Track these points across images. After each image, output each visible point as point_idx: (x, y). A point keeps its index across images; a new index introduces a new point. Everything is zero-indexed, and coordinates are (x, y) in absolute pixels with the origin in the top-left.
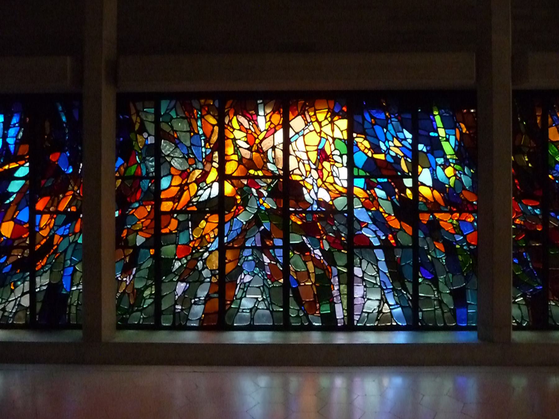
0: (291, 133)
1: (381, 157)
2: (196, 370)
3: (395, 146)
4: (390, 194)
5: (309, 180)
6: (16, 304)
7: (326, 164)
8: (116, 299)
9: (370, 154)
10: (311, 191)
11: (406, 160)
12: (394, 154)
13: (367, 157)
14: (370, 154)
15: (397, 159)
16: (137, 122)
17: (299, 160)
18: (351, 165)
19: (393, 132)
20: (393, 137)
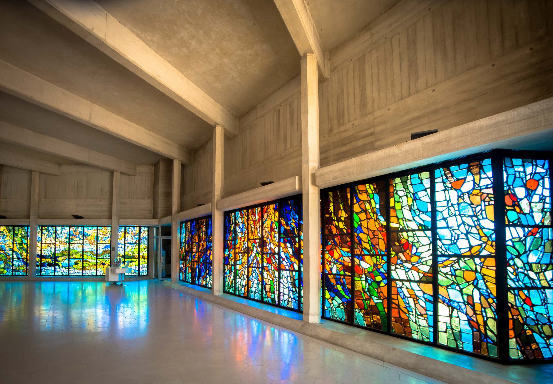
0: (264, 220)
1: (288, 228)
2: (336, 349)
3: (293, 222)
4: (292, 245)
5: (268, 240)
6: (534, 334)
7: (273, 232)
8: (302, 303)
9: (285, 227)
10: (477, 231)
11: (296, 229)
12: (292, 226)
13: (493, 206)
14: (285, 227)
15: (293, 228)
16: (516, 177)
17: (266, 231)
18: (279, 233)
19: (292, 216)
20: (292, 218)
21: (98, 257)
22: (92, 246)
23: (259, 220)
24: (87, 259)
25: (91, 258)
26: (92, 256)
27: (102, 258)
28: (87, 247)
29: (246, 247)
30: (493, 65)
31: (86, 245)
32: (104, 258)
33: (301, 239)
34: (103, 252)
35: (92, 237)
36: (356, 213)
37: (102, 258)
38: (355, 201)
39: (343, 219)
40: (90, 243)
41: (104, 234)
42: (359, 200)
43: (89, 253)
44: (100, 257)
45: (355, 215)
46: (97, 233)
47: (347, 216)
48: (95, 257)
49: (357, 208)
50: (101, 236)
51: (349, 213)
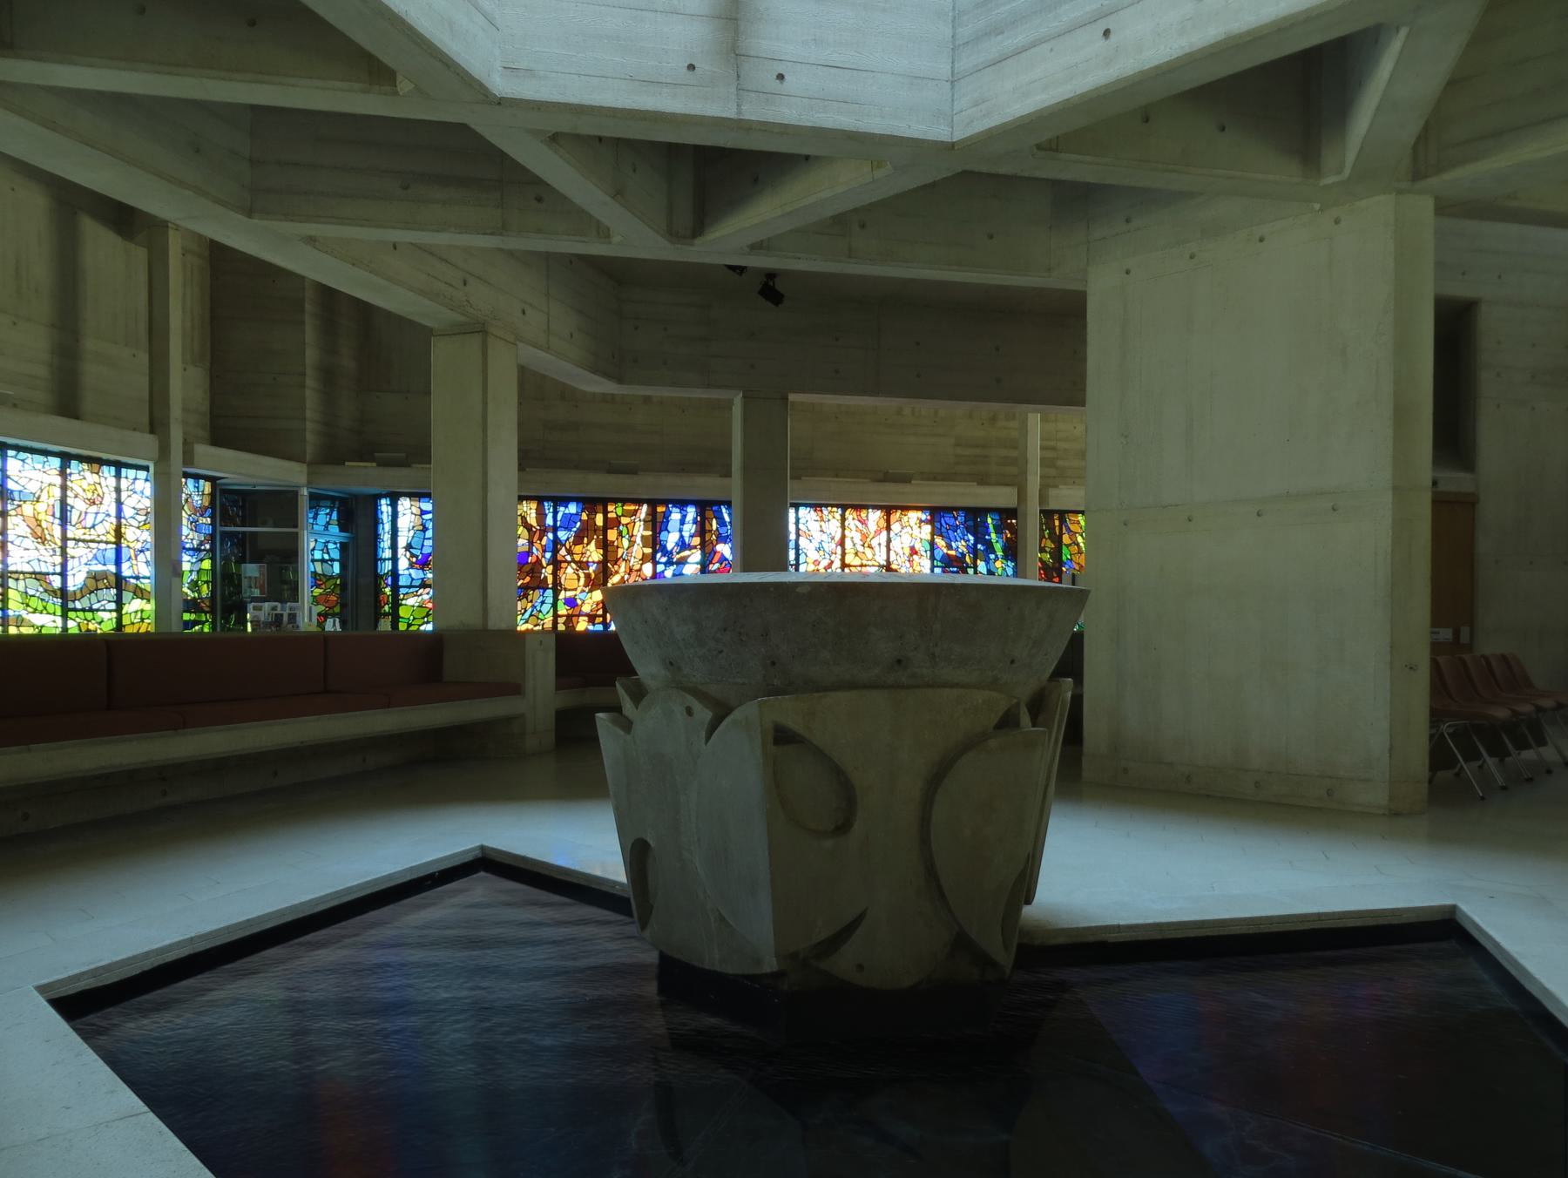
15: (963, 555)
18: (932, 558)
21: (71, 605)
22: (41, 547)
23: (878, 532)
24: (24, 614)
25: (40, 608)
26: (45, 596)
27: (83, 610)
28: (22, 552)
29: (390, 568)
30: (781, 77)
31: (17, 542)
32: (91, 610)
33: (67, 505)
34: (91, 583)
35: (41, 507)
36: (1065, 545)
37: (83, 610)
38: (1064, 531)
39: (1048, 550)
40: (34, 534)
41: (89, 495)
42: (1069, 530)
43: (32, 582)
44: (78, 605)
45: (1064, 548)
46: (64, 488)
47: (1053, 546)
48: (55, 604)
49: (1066, 539)
50: (77, 505)
51: (1057, 544)
